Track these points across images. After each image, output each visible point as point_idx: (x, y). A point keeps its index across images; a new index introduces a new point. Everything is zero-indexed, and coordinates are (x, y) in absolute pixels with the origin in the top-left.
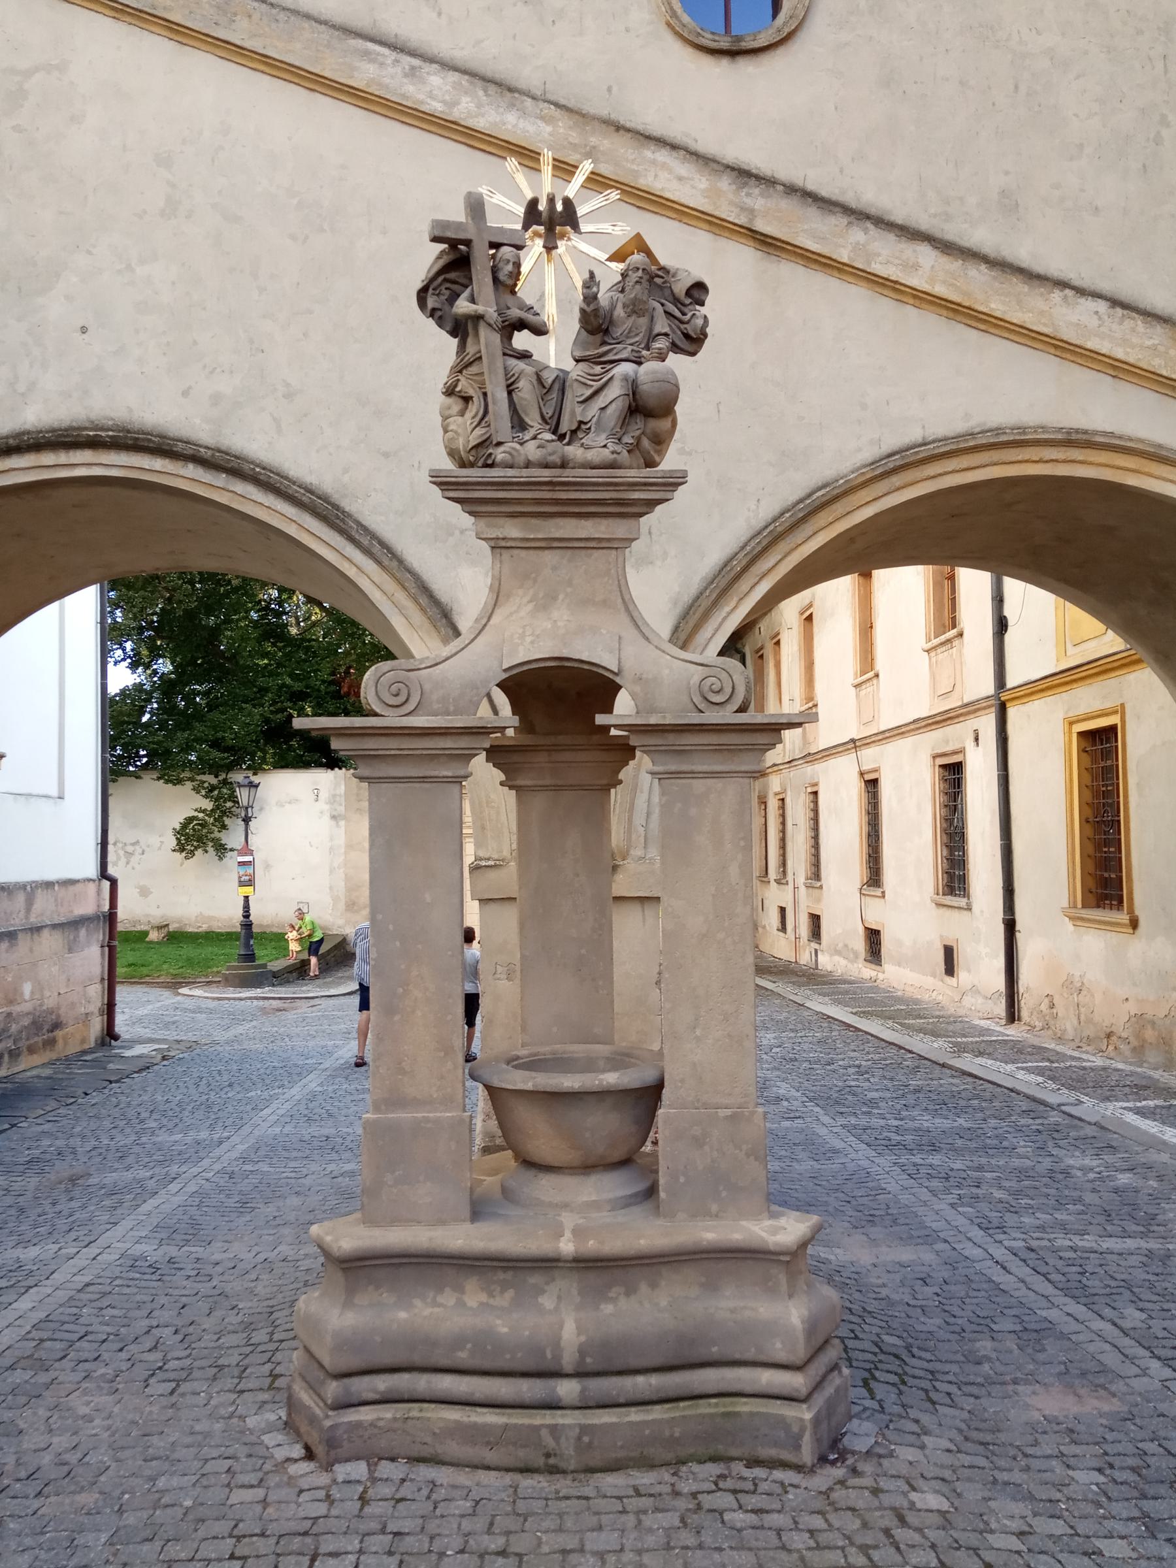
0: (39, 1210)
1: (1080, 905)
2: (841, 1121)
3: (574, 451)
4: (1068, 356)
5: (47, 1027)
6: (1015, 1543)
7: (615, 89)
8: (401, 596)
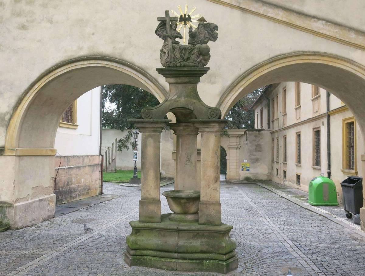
1: (345, 168)
2: (271, 219)
5: (88, 189)
8: (158, 91)
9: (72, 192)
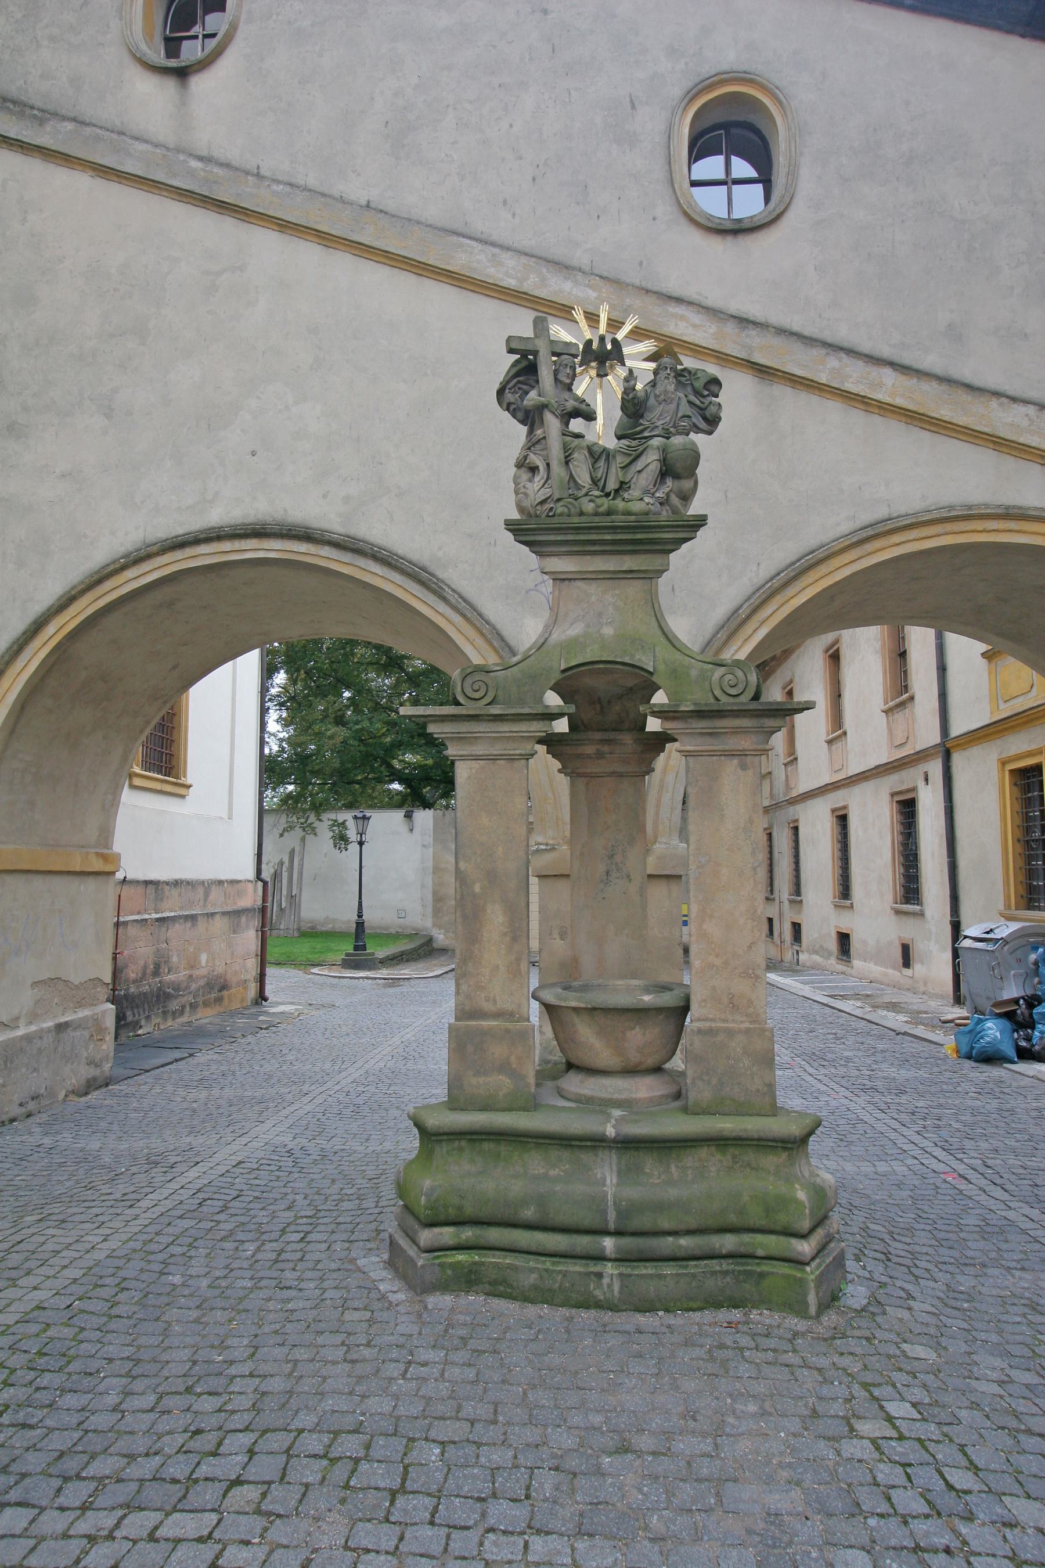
0: (207, 1112)
1: (1013, 908)
2: (823, 1071)
3: (620, 504)
4: (1005, 450)
6: (996, 1389)
7: (645, 263)
9: (168, 997)
